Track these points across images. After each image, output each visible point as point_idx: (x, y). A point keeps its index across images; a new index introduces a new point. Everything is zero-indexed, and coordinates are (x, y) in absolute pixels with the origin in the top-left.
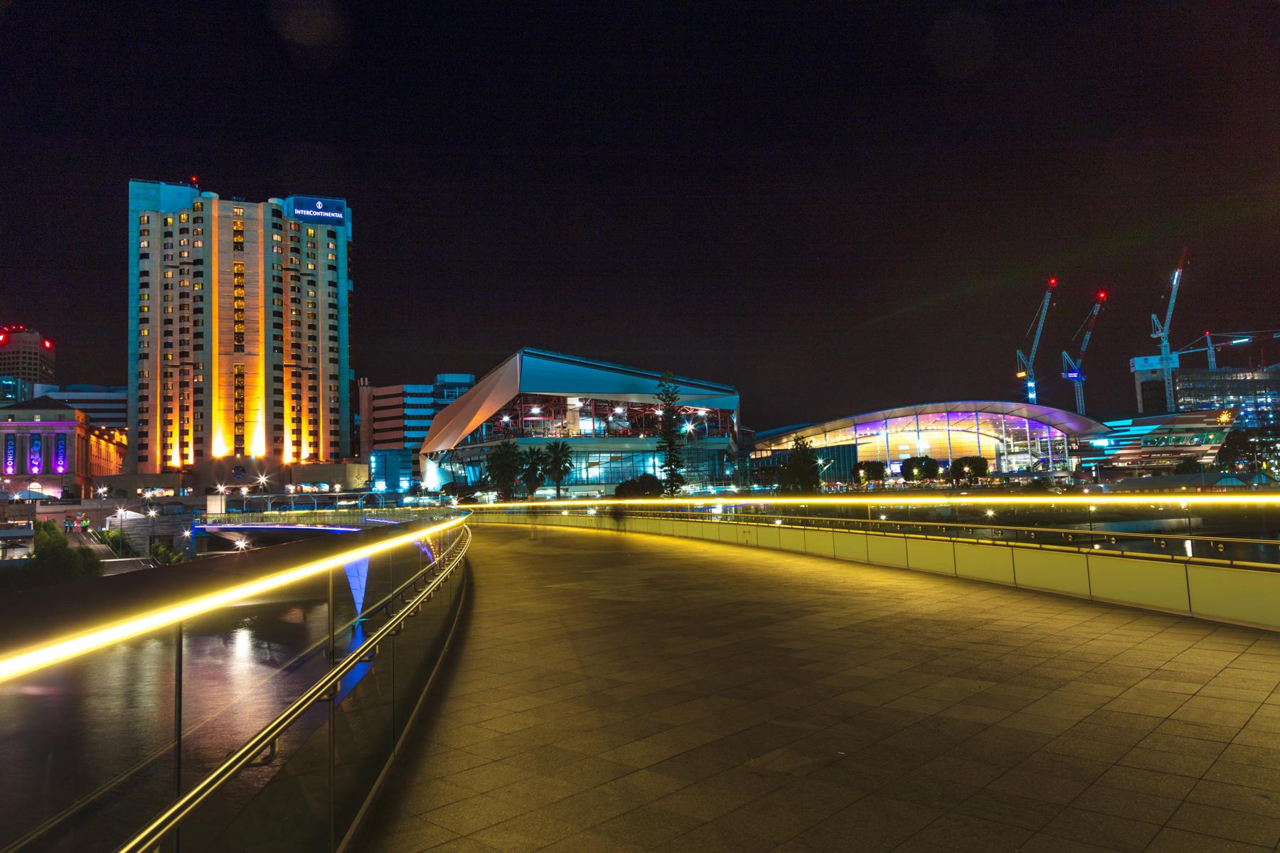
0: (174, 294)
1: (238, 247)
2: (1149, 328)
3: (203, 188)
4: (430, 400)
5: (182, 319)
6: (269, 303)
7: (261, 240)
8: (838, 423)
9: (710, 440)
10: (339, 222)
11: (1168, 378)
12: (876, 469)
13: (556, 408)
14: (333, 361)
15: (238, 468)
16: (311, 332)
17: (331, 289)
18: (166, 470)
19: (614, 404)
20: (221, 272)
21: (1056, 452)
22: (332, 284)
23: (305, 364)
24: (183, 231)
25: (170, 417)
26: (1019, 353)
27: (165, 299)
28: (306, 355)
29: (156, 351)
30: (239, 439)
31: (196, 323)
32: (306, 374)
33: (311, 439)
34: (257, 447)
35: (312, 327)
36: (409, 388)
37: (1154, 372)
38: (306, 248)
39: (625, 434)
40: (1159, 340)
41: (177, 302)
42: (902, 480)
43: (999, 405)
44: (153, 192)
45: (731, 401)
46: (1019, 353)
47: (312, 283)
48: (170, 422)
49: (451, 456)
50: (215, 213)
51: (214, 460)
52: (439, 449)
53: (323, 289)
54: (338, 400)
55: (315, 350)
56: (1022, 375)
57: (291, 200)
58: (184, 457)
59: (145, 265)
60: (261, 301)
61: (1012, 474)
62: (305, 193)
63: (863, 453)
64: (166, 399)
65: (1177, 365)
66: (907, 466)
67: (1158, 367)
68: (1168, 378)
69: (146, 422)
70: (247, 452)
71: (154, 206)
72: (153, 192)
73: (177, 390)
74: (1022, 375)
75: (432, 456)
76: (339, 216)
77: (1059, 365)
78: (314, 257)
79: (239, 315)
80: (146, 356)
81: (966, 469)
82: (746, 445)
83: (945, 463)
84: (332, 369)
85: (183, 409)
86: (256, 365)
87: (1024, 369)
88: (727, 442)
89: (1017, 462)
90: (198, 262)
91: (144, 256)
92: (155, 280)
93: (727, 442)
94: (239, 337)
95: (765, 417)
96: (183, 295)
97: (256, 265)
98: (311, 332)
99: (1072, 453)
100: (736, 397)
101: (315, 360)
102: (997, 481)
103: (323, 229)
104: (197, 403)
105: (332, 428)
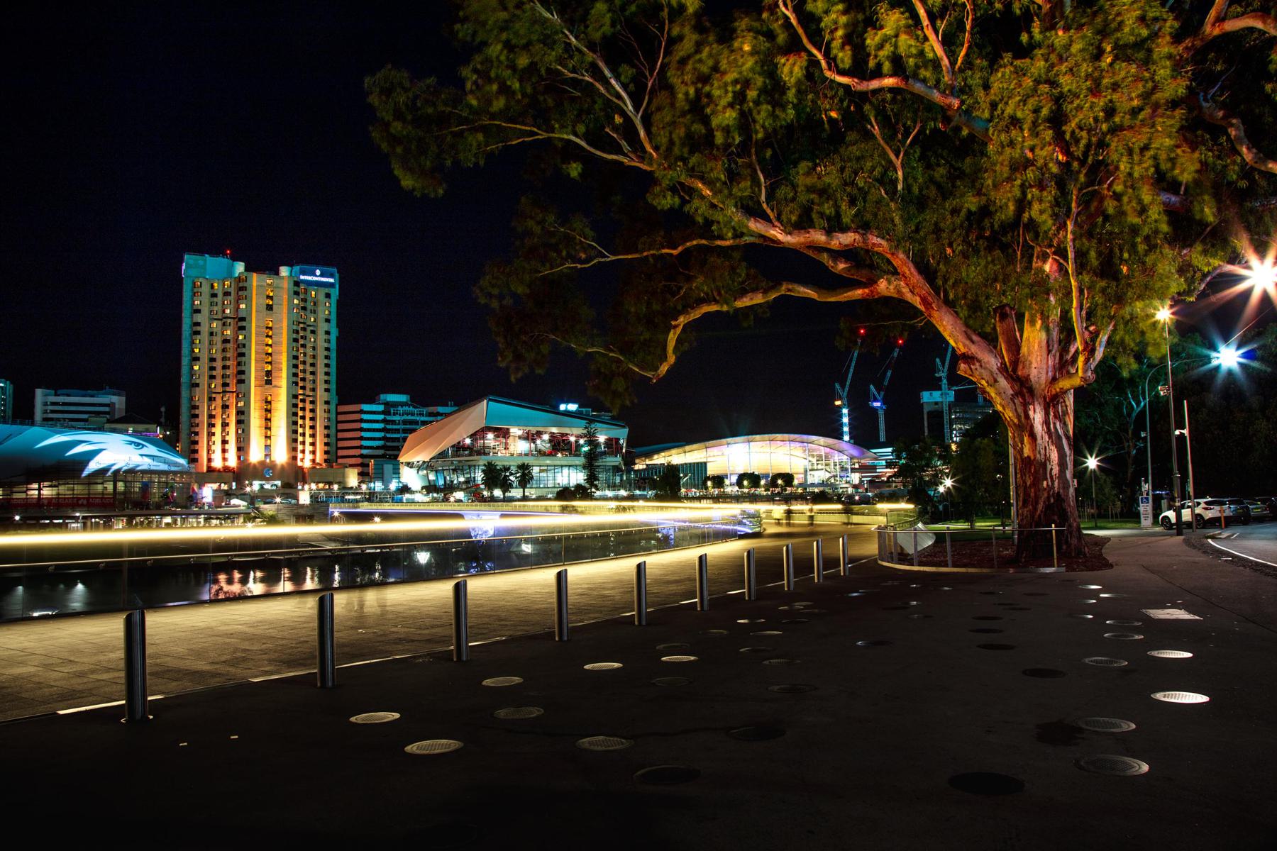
0: (218, 339)
1: (270, 308)
2: (934, 370)
3: (235, 258)
4: (381, 417)
5: (224, 359)
6: (290, 349)
7: (285, 303)
8: (695, 446)
9: (608, 459)
10: (332, 285)
11: (946, 408)
12: (719, 480)
13: (503, 433)
14: (327, 390)
15: (262, 471)
16: (311, 369)
17: (327, 337)
18: (211, 470)
19: (539, 434)
20: (257, 326)
21: (843, 469)
22: (328, 333)
23: (308, 392)
24: (227, 294)
25: (213, 430)
26: (837, 385)
27: (211, 343)
28: (309, 386)
29: (204, 381)
30: (267, 447)
31: (239, 364)
32: (308, 399)
33: (311, 448)
34: (280, 456)
35: (313, 365)
36: (366, 407)
37: (936, 403)
38: (310, 305)
39: (550, 454)
40: (940, 379)
41: (219, 346)
42: (736, 488)
43: (805, 437)
44: (201, 262)
45: (622, 434)
46: (837, 385)
47: (313, 332)
48: (214, 434)
49: (427, 466)
50: (255, 284)
51: (282, 466)
52: (415, 460)
53: (321, 336)
54: (329, 419)
55: (314, 382)
56: (838, 403)
57: (297, 268)
58: (225, 459)
59: (198, 318)
60: (284, 348)
61: (813, 485)
62: (311, 263)
63: (712, 470)
64: (211, 416)
65: (952, 399)
66: (742, 477)
67: (939, 400)
68: (946, 408)
69: (197, 434)
70: (246, 460)
71: (206, 273)
72: (201, 262)
73: (220, 410)
74: (838, 403)
75: (410, 465)
76: (332, 280)
77: (867, 397)
78: (314, 312)
79: (268, 358)
80: (197, 385)
81: (780, 482)
82: (629, 460)
83: (766, 476)
84: (326, 396)
85: (225, 425)
86: (278, 395)
87: (840, 399)
88: (617, 460)
89: (817, 477)
90: (243, 319)
91: (198, 311)
92: (204, 329)
93: (617, 460)
94: (269, 373)
95: (644, 441)
96: (226, 341)
97: (281, 321)
98: (311, 369)
99: (853, 470)
100: (626, 431)
101: (313, 390)
102: (800, 491)
103: (323, 291)
104: (239, 422)
105: (326, 440)
